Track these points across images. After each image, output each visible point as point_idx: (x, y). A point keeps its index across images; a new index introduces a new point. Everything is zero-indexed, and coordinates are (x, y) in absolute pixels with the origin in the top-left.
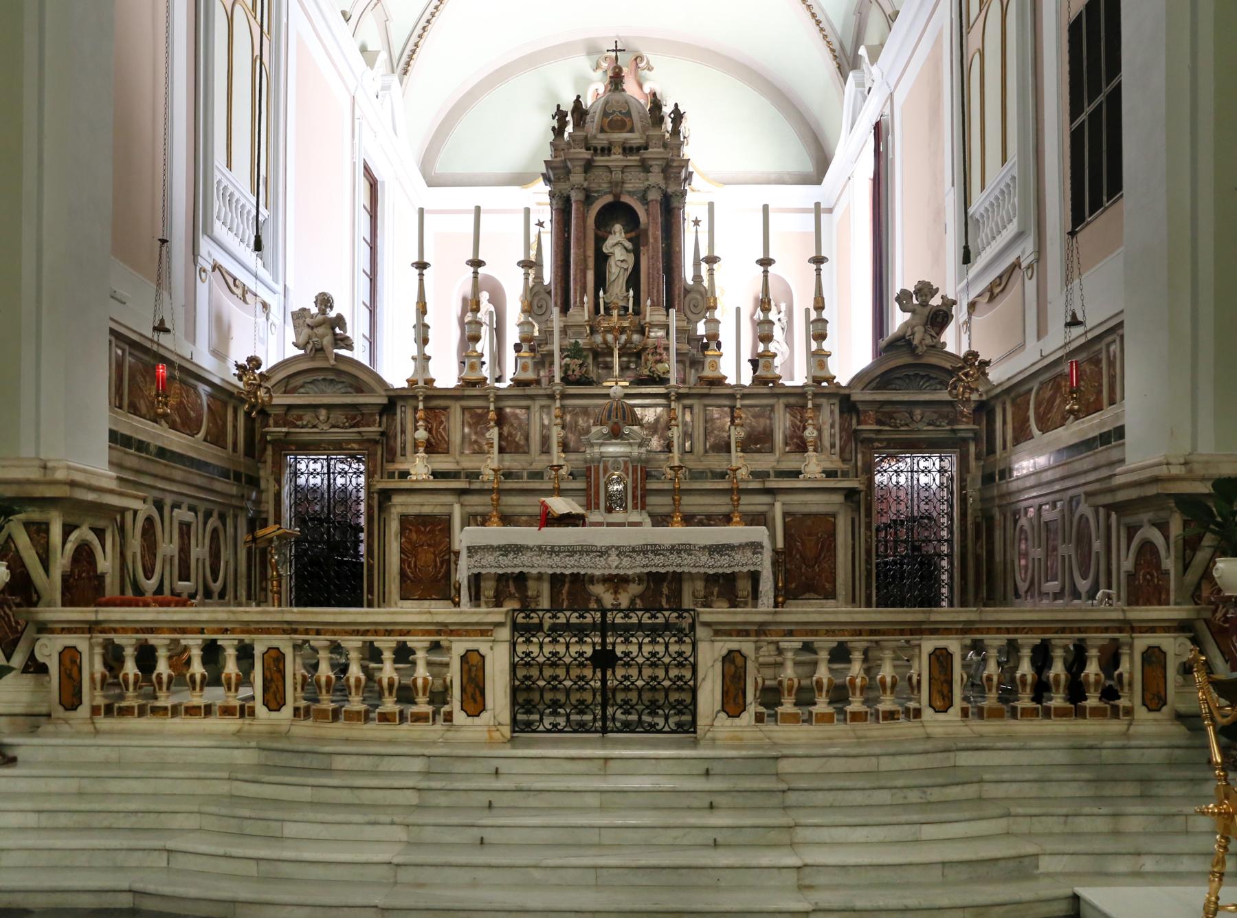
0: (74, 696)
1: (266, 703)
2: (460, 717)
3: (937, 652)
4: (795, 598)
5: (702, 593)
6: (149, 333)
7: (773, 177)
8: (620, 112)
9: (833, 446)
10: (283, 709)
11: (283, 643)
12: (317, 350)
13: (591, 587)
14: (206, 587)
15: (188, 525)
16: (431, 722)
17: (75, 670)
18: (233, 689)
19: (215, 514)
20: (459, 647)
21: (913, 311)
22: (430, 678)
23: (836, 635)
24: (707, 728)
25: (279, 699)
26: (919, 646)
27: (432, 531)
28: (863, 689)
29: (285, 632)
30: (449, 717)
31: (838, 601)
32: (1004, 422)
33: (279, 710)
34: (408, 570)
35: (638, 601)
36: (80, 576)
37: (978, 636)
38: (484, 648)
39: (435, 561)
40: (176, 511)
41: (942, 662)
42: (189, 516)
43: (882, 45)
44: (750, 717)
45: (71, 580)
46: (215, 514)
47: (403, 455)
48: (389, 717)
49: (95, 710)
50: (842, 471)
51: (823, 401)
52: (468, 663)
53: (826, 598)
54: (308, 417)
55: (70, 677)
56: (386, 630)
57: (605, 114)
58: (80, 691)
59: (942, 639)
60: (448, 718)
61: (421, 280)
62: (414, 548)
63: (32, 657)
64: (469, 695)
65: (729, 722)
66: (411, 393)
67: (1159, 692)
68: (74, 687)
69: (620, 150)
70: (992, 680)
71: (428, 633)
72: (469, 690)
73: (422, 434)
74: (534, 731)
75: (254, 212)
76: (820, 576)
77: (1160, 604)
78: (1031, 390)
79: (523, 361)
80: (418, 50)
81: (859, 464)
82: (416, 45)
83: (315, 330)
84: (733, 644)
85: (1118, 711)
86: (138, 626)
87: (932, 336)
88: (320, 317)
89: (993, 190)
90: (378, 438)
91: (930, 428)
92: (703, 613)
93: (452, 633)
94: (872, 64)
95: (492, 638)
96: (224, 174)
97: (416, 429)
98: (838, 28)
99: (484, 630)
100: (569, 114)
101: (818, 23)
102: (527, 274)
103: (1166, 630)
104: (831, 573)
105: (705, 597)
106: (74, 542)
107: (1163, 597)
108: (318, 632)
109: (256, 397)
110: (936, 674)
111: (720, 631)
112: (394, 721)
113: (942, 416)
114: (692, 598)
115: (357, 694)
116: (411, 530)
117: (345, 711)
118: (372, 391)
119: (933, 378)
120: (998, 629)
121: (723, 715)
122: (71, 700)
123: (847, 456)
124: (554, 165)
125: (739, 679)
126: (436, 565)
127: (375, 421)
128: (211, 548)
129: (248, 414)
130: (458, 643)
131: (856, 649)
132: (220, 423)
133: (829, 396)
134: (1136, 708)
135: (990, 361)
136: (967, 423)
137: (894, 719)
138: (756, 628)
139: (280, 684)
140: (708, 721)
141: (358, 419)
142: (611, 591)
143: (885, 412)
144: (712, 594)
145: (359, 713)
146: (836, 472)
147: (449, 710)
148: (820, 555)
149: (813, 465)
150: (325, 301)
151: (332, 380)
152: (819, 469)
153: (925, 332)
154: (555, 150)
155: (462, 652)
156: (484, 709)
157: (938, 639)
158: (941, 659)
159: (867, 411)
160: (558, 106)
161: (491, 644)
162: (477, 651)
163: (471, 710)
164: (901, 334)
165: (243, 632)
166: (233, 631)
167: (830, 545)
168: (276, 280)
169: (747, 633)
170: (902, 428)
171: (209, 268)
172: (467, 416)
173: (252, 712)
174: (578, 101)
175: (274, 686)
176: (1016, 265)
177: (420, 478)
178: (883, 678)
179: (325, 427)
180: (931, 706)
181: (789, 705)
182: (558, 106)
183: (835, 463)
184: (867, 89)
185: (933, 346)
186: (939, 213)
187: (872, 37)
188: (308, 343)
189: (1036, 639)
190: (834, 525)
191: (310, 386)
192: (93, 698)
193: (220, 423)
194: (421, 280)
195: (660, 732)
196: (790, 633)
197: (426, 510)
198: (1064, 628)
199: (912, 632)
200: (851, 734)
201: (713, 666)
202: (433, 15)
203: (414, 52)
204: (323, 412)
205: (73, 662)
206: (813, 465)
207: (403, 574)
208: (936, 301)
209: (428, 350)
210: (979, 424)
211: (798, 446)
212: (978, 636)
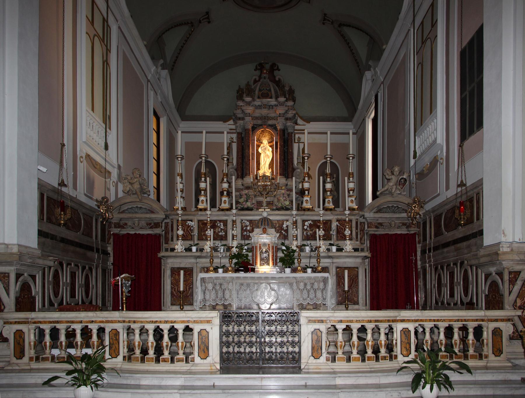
0: (21, 352)
2: (198, 360)
6: (56, 186)
17: (21, 340)
25: (116, 353)
31: (359, 305)
34: (174, 292)
36: (24, 297)
41: (406, 334)
45: (20, 299)
47: (172, 240)
49: (31, 359)
52: (201, 335)
53: (354, 304)
55: (19, 344)
58: (24, 350)
60: (193, 360)
63: (387, 179)
64: (202, 350)
65: (315, 361)
67: (500, 348)
68: (21, 348)
73: (180, 232)
76: (352, 294)
77: (499, 309)
84: (317, 326)
85: (482, 356)
86: (51, 320)
97: (178, 230)
103: (502, 320)
106: (21, 282)
107: (501, 305)
108: (134, 322)
110: (404, 340)
111: (311, 321)
112: (169, 362)
116: (176, 274)
119: (399, 208)
120: (430, 320)
121: (312, 358)
122: (20, 353)
123: (363, 242)
127: (160, 225)
129: (102, 222)
134: (490, 356)
137: (386, 360)
139: (117, 346)
145: (153, 358)
146: (358, 249)
158: (405, 332)
160: (240, 86)
163: (203, 356)
167: (356, 281)
175: (114, 346)
182: (240, 86)
189: (446, 324)
192: (30, 353)
198: (459, 319)
205: (21, 337)
206: (348, 246)
207: (172, 294)
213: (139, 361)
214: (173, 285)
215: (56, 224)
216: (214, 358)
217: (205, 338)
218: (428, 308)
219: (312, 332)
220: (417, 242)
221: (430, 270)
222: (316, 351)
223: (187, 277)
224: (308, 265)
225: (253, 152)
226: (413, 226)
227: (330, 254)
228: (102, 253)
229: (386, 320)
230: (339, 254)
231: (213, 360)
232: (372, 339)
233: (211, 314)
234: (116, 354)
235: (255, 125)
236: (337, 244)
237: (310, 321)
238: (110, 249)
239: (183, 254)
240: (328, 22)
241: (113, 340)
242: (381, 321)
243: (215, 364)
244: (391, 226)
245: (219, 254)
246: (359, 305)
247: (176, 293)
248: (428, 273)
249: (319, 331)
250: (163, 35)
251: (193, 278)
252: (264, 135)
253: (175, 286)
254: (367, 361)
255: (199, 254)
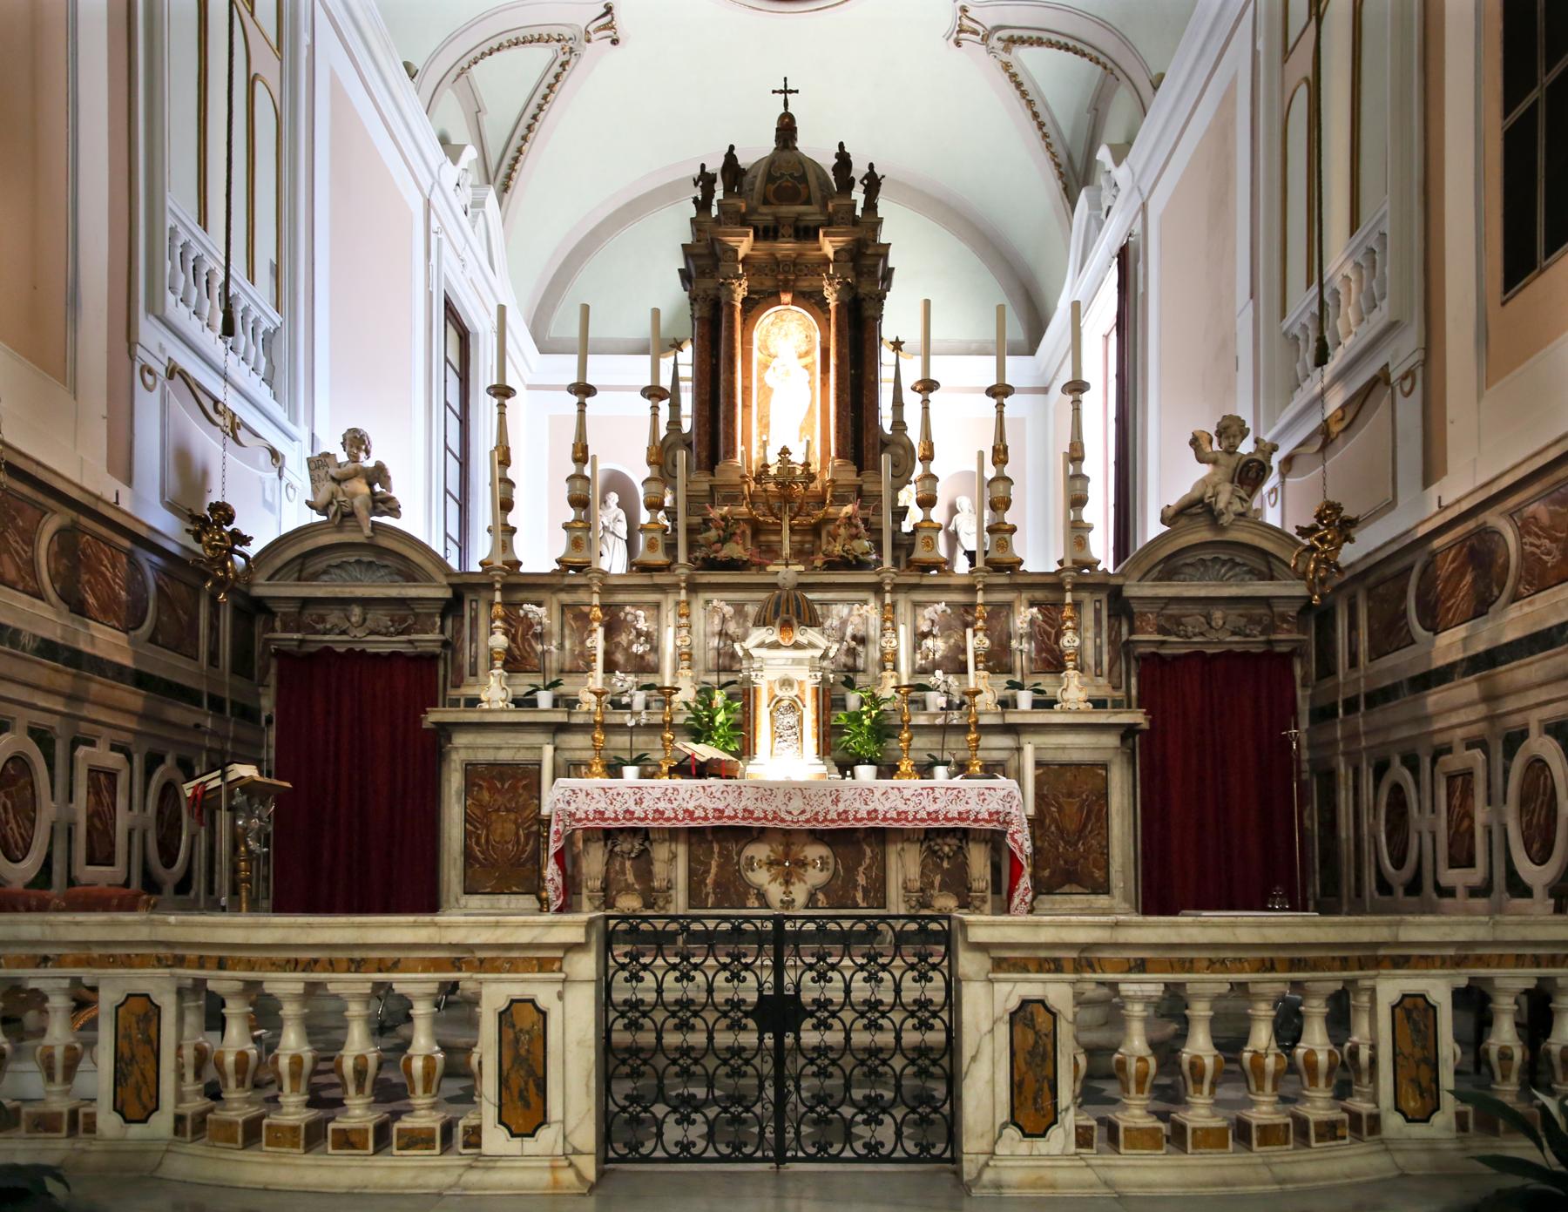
1: (118, 1108)
2: (495, 1139)
3: (1407, 1002)
4: (1050, 893)
5: (918, 885)
7: (974, 346)
8: (791, 175)
9: (1098, 664)
10: (154, 1118)
11: (159, 985)
12: (344, 516)
13: (750, 874)
14: (146, 873)
15: (112, 775)
16: (437, 1150)
18: (59, 1077)
19: (170, 760)
20: (495, 993)
21: (1215, 462)
22: (441, 1056)
23: (1228, 971)
24: (983, 1158)
25: (145, 1097)
26: (1373, 990)
27: (513, 788)
28: (1277, 1077)
29: (160, 962)
30: (474, 1137)
31: (1113, 897)
32: (1353, 626)
33: (145, 1121)
35: (821, 896)
37: (1482, 972)
38: (544, 995)
39: (517, 834)
40: (82, 751)
41: (1415, 1023)
42: (114, 760)
43: (1129, 143)
44: (1067, 1136)
46: (170, 760)
47: (474, 674)
48: (354, 1138)
50: (1114, 701)
51: (1084, 596)
52: (513, 1026)
53: (1095, 892)
54: (334, 617)
56: (352, 960)
57: (770, 178)
59: (1417, 976)
60: (473, 1139)
61: (502, 414)
62: (486, 814)
64: (516, 1094)
65: (1024, 1147)
66: (484, 580)
69: (791, 231)
70: (1511, 1058)
71: (436, 965)
72: (516, 1081)
74: (646, 1159)
75: (220, 277)
76: (1086, 859)
78: (1411, 568)
79: (650, 535)
80: (522, 158)
81: (1134, 692)
82: (520, 151)
83: (343, 486)
87: (1240, 498)
88: (351, 466)
89: (1299, 316)
90: (438, 650)
91: (1236, 638)
92: (974, 924)
93: (482, 965)
94: (1118, 163)
95: (562, 976)
96: (243, 290)
98: (1066, 132)
99: (546, 960)
100: (719, 178)
101: (1041, 125)
102: (655, 408)
104: (1102, 854)
105: (922, 890)
108: (221, 964)
109: (225, 570)
110: (1406, 1048)
111: (1005, 961)
112: (365, 1147)
113: (1252, 620)
114: (902, 892)
115: (294, 1090)
116: (480, 787)
117: (269, 1126)
118: (429, 579)
119: (1238, 564)
120: (1518, 957)
121: (1012, 1133)
124: (697, 251)
125: (1044, 1057)
126: (518, 842)
128: (160, 812)
130: (494, 987)
131: (1261, 997)
132: (185, 618)
133: (1094, 587)
135: (1357, 519)
136: (1289, 631)
137: (1335, 1138)
138: (1074, 955)
140: (984, 1145)
141: (410, 622)
142: (780, 880)
143: (1171, 616)
144: (932, 885)
145: (294, 1129)
147: (474, 1122)
148: (1085, 826)
149: (1074, 690)
150: (356, 441)
151: (370, 563)
152: (1083, 696)
153: (1232, 493)
154: (698, 230)
155: (502, 1004)
156: (543, 1121)
157: (1408, 977)
158: (1413, 1012)
159: (1145, 614)
161: (559, 987)
162: (532, 1001)
163: (518, 1122)
164: (1197, 495)
165: (78, 963)
166: (59, 962)
167: (1100, 810)
168: (294, 419)
169: (1057, 966)
170: (1195, 639)
171: (161, 370)
172: (569, 616)
173: (91, 1127)
174: (730, 157)
176: (1381, 380)
177: (494, 706)
178: (1311, 1053)
179: (360, 633)
180: (1397, 1109)
181: (1137, 1112)
182: (703, 166)
183: (1103, 689)
184: (1105, 209)
185: (1242, 515)
186: (1224, 347)
187: (1114, 131)
188: (331, 503)
190: (1106, 780)
191: (338, 571)
193: (185, 618)
194: (502, 414)
195: (887, 1159)
196: (1141, 966)
197: (505, 756)
199: (1362, 964)
200: (1265, 1173)
201: (992, 1031)
202: (540, 108)
203: (516, 160)
204: (357, 611)
206: (1074, 690)
207: (468, 854)
208: (1246, 447)
209: (512, 519)
210: (1304, 631)
211: (1048, 663)
212: (1482, 972)
213: (236, 1142)
214: (471, 824)
215: (20, 587)
216: (572, 1132)
217: (531, 1041)
218: (1345, 908)
219: (1013, 1015)
220: (1298, 681)
221: (1351, 776)
222: (1030, 1102)
223: (520, 795)
224: (936, 754)
225: (747, 384)
226: (1285, 626)
227: (1012, 718)
228: (232, 714)
229: (1334, 958)
230: (1041, 717)
231: (565, 1138)
232: (1274, 1044)
233: (555, 930)
234: (145, 1108)
235: (756, 292)
236: (1036, 685)
237: (1005, 966)
238: (267, 704)
239: (506, 718)
240: (973, 37)
241: (130, 1043)
242: (1314, 965)
243: (574, 1158)
244: (1211, 627)
245: (628, 717)
246: (1113, 897)
247: (482, 853)
248: (1342, 787)
249: (1042, 1009)
250: (474, 67)
251: (539, 799)
252: (783, 332)
253: (477, 829)
254: (1260, 1144)
255: (560, 717)
